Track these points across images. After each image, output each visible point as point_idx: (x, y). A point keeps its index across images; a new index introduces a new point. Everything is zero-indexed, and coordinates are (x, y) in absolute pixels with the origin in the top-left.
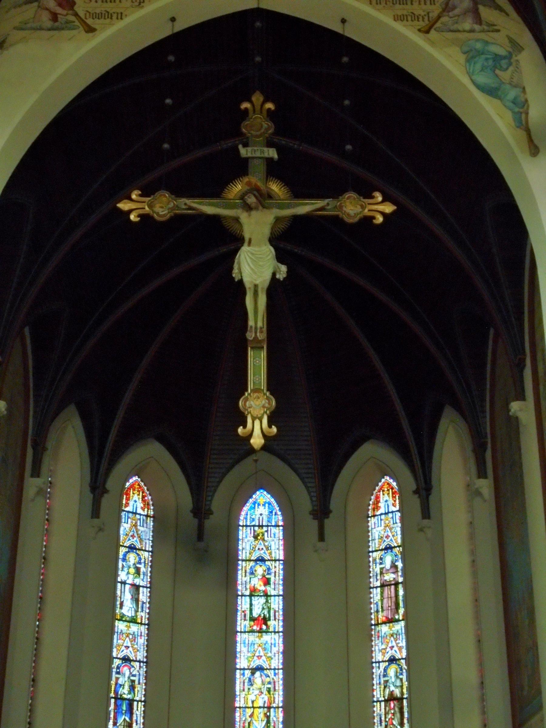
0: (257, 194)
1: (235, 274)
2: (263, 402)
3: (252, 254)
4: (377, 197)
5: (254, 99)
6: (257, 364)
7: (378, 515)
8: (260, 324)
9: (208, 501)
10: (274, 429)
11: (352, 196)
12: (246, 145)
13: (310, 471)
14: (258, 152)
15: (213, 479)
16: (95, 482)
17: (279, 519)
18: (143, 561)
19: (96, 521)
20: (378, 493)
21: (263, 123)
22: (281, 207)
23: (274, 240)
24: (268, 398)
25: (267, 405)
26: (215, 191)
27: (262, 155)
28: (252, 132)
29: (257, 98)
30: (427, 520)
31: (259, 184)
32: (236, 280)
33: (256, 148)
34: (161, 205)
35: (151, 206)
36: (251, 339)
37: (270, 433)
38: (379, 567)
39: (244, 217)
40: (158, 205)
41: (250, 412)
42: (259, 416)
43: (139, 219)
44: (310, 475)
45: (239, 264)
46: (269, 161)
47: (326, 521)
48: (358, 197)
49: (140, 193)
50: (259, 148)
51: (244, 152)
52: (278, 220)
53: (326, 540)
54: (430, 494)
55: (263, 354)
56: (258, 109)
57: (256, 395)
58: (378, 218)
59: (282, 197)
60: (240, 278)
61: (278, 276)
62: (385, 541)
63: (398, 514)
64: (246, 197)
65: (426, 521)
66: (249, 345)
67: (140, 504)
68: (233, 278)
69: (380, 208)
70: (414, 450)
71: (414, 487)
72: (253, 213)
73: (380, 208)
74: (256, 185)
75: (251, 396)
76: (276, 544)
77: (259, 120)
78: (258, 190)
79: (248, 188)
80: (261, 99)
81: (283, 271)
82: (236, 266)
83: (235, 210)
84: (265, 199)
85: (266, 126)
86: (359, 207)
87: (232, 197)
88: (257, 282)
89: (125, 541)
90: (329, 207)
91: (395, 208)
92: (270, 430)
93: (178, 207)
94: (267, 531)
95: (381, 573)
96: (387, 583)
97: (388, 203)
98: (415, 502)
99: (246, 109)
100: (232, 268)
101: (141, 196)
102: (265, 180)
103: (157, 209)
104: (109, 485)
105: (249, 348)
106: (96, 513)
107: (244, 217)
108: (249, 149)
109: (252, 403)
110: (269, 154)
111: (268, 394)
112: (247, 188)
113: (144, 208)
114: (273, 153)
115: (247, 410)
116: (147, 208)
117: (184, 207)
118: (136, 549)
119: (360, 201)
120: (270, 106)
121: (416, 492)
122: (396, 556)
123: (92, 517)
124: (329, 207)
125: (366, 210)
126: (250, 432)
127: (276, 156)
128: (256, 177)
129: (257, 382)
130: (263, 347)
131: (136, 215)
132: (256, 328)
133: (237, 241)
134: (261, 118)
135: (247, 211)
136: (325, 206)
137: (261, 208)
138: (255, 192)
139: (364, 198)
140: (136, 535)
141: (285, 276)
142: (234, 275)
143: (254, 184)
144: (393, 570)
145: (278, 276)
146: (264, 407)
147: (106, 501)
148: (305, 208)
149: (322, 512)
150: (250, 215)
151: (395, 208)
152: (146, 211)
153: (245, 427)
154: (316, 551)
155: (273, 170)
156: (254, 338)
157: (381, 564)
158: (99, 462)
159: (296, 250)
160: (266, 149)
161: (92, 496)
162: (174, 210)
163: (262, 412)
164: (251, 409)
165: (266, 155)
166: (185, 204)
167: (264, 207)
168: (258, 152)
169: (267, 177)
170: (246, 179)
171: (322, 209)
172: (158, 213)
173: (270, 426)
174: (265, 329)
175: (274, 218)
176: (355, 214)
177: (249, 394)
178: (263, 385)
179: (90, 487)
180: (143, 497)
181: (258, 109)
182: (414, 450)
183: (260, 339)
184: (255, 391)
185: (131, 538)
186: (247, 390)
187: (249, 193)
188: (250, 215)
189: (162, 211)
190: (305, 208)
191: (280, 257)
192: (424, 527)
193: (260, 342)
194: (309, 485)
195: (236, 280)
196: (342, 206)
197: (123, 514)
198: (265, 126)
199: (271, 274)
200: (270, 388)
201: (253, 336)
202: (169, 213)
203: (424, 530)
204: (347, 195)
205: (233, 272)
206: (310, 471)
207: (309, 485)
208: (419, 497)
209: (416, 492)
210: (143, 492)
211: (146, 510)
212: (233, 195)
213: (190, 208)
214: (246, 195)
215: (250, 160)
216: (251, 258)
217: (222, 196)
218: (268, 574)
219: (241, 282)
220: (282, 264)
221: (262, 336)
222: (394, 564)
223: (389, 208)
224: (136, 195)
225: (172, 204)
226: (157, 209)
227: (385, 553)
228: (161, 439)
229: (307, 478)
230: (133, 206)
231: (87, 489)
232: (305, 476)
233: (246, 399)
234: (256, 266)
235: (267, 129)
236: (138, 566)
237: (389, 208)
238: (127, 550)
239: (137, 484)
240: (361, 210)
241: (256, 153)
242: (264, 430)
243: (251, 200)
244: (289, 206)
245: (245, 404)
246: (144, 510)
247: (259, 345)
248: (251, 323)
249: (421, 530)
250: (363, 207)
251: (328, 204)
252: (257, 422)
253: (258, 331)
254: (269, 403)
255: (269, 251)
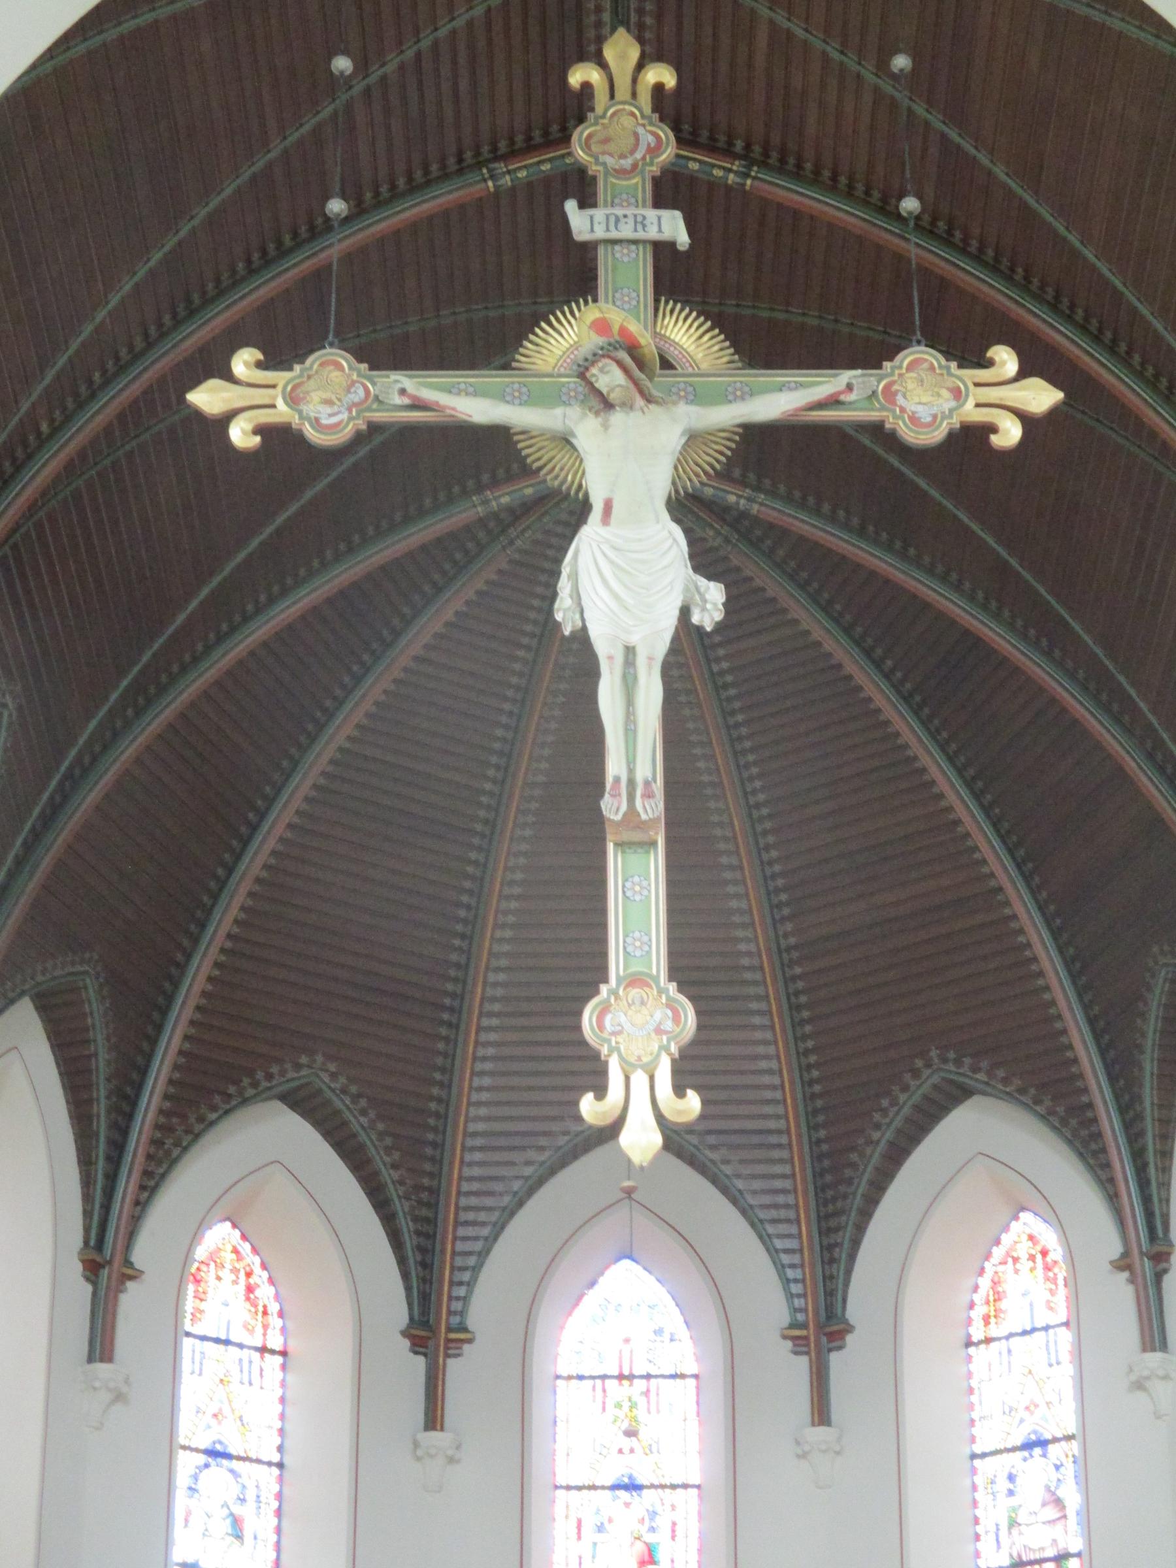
0: (628, 360)
1: (564, 612)
2: (658, 1015)
3: (615, 548)
4: (1004, 363)
5: (609, 53)
6: (637, 899)
7: (999, 1339)
8: (643, 771)
9: (458, 1298)
10: (693, 1103)
11: (926, 360)
12: (587, 202)
13: (781, 1199)
14: (624, 223)
15: (470, 1231)
16: (100, 1245)
17: (683, 1353)
18: (251, 1495)
19: (101, 1368)
20: (1001, 1268)
21: (640, 130)
22: (697, 397)
23: (686, 507)
24: (671, 1005)
25: (669, 1025)
26: (491, 345)
27: (641, 235)
28: (610, 161)
29: (621, 50)
30: (1159, 1355)
31: (634, 327)
32: (567, 632)
33: (619, 212)
34: (326, 395)
35: (293, 400)
36: (618, 817)
37: (680, 1112)
38: (1005, 1503)
39: (587, 431)
40: (316, 396)
41: (618, 1050)
42: (645, 1060)
43: (258, 439)
44: (783, 1214)
45: (574, 577)
46: (662, 250)
47: (834, 1357)
48: (943, 361)
49: (260, 356)
50: (629, 212)
51: (582, 223)
52: (694, 438)
53: (834, 1417)
54: (1165, 1271)
55: (655, 864)
56: (622, 87)
57: (634, 992)
58: (1007, 432)
59: (704, 366)
60: (580, 624)
61: (696, 619)
62: (1022, 1421)
63: (1065, 1337)
64: (594, 371)
65: (1154, 1359)
66: (609, 837)
67: (240, 1310)
68: (558, 625)
69: (1008, 398)
70: (1110, 1123)
71: (1115, 1249)
72: (617, 418)
73: (1008, 398)
74: (623, 330)
75: (617, 997)
76: (678, 1437)
77: (627, 122)
78: (633, 349)
79: (600, 340)
80: (634, 53)
81: (711, 603)
82: (564, 586)
83: (559, 411)
84: (650, 368)
85: (651, 138)
86: (945, 394)
87: (548, 369)
88: (634, 639)
89: (193, 1428)
90: (852, 397)
91: (1059, 395)
92: (681, 1104)
93: (381, 402)
94: (647, 1393)
95: (1013, 1523)
96: (1032, 1557)
97: (1036, 382)
98: (1120, 1294)
99: (587, 86)
100: (552, 596)
101: (259, 365)
102: (651, 311)
103: (315, 407)
104: (143, 1253)
105: (610, 847)
106: (101, 1346)
107: (587, 431)
108: (599, 214)
109: (623, 1019)
110: (660, 231)
111: (672, 987)
112: (595, 340)
113: (273, 406)
114: (673, 227)
115: (609, 1041)
116: (281, 404)
117: (398, 400)
118: (227, 1456)
119: (950, 374)
120: (662, 75)
121: (1123, 1264)
122: (1057, 1467)
123: (90, 1360)
124: (852, 397)
125: (970, 405)
126: (617, 1112)
127: (683, 239)
128: (622, 301)
129: (638, 953)
130: (653, 844)
131: (249, 427)
132: (631, 783)
133: (570, 511)
134: (633, 114)
135: (597, 414)
136: (840, 393)
137: (640, 402)
138: (623, 355)
139: (960, 367)
140: (226, 1410)
141: (718, 616)
142: (559, 617)
143: (616, 329)
144: (1051, 1513)
145: (696, 619)
146: (659, 1031)
147: (132, 1302)
148: (781, 398)
149: (822, 1327)
150: (606, 426)
151: (1059, 395)
152: (281, 414)
153: (601, 1091)
154: (803, 1456)
155: (674, 278)
156: (625, 815)
157: (1011, 1493)
158: (111, 1179)
159: (732, 499)
160: (652, 214)
161: (89, 1288)
162: (369, 409)
163: (655, 1047)
164: (620, 1039)
165: (652, 234)
166: (403, 392)
167: (649, 399)
168: (624, 223)
169: (657, 301)
170: (591, 313)
171: (833, 402)
172: (317, 419)
173: (679, 1091)
174: (659, 786)
175: (683, 434)
176: (935, 417)
177: (614, 993)
178: (658, 963)
179: (83, 1261)
180: (250, 1289)
181: (622, 87)
182: (1110, 1123)
183: (644, 817)
184: (635, 981)
185: (213, 1422)
186: (606, 980)
187: (603, 356)
188: (606, 426)
189: (330, 415)
190: (781, 398)
191: (703, 561)
192: (1148, 1378)
193: (642, 826)
194: (779, 1244)
195: (567, 632)
196: (896, 393)
197: (187, 1343)
198: (647, 139)
199: (676, 613)
200: (675, 973)
201: (624, 807)
202: (351, 419)
203: (1148, 1384)
204: (906, 357)
205: (556, 606)
206: (781, 1199)
207: (779, 1244)
208: (1132, 1281)
209: (1123, 1264)
210: (249, 1275)
211: (259, 1330)
212: (552, 361)
213: (418, 405)
214: (593, 363)
215: (601, 251)
216: (612, 562)
217: (514, 364)
218: (652, 1529)
219: (582, 638)
220: (710, 578)
221: (652, 808)
222: (1054, 1494)
223: (1041, 397)
224: (246, 364)
225: (361, 392)
226: (315, 407)
227: (1025, 1460)
228: (304, 1103)
229: (774, 1221)
230: (243, 399)
231: (77, 1268)
232: (762, 1214)
233: (604, 1010)
234: (631, 588)
235: (654, 151)
236: (237, 1510)
237: (1041, 397)
238: (202, 1459)
239: (230, 1248)
240: (953, 404)
241: (621, 226)
242: (667, 1113)
243: (610, 378)
244: (726, 397)
245: (601, 1026)
246: (251, 1331)
247: (637, 836)
248: (614, 766)
249: (1139, 1385)
250: (957, 394)
251: (850, 387)
252: (639, 1080)
253: (639, 793)
254: (676, 1019)
255: (670, 541)
